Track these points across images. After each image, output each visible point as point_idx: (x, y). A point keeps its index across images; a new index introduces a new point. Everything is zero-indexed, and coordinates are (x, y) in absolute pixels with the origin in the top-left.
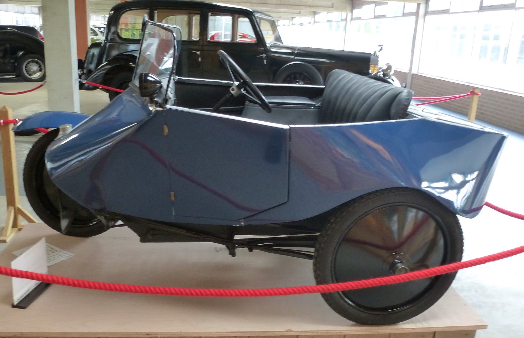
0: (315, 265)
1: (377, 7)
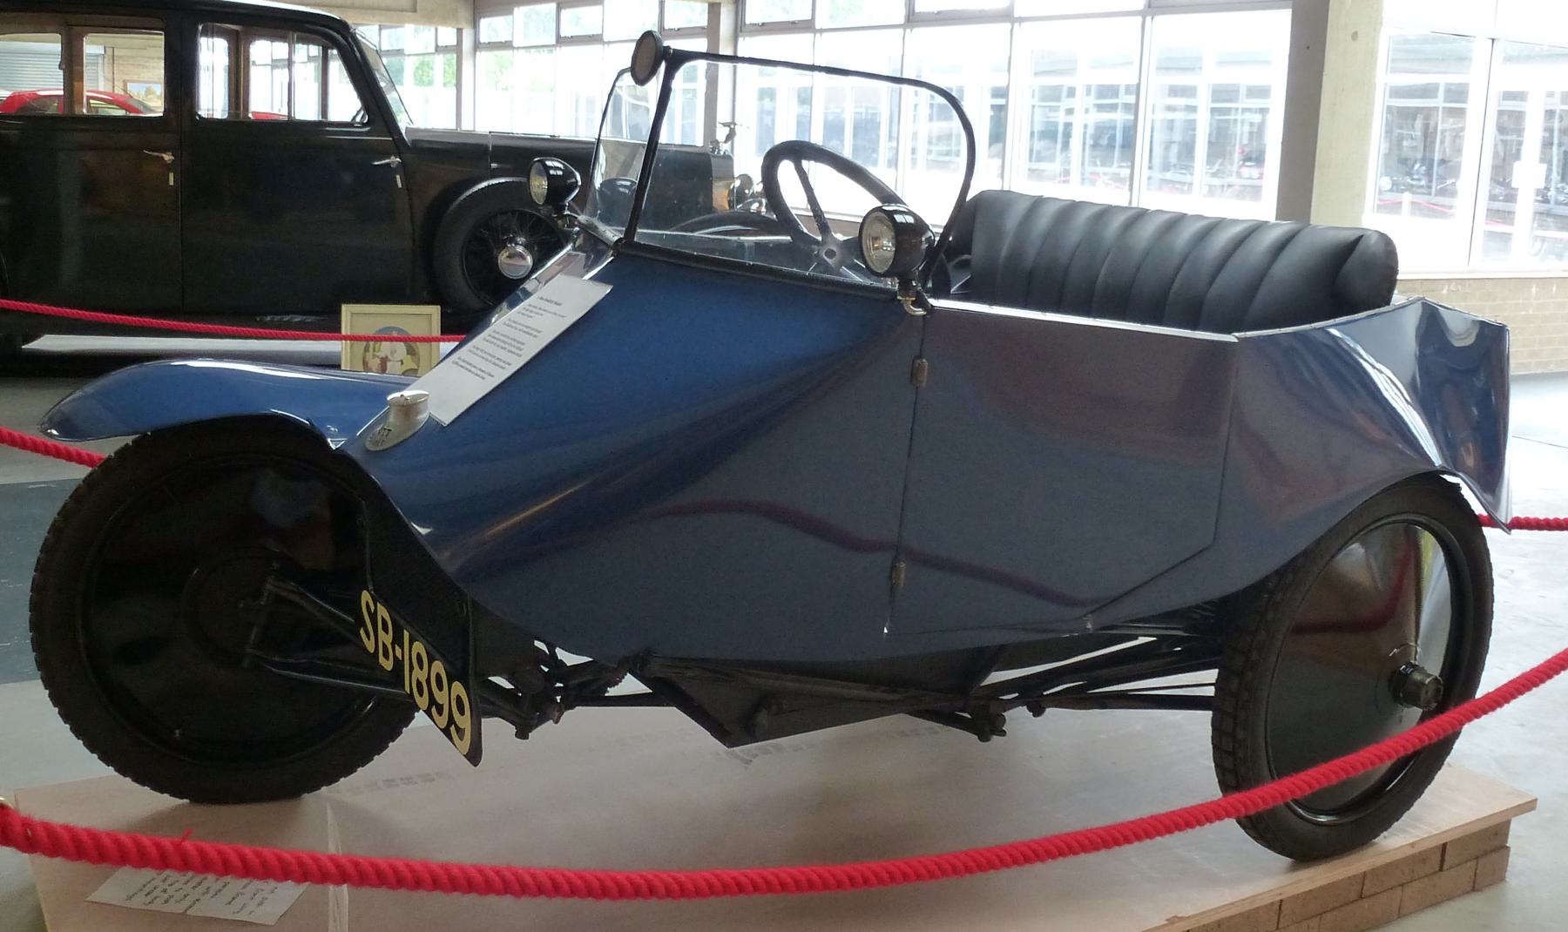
0: (1216, 726)
1: (384, 32)
